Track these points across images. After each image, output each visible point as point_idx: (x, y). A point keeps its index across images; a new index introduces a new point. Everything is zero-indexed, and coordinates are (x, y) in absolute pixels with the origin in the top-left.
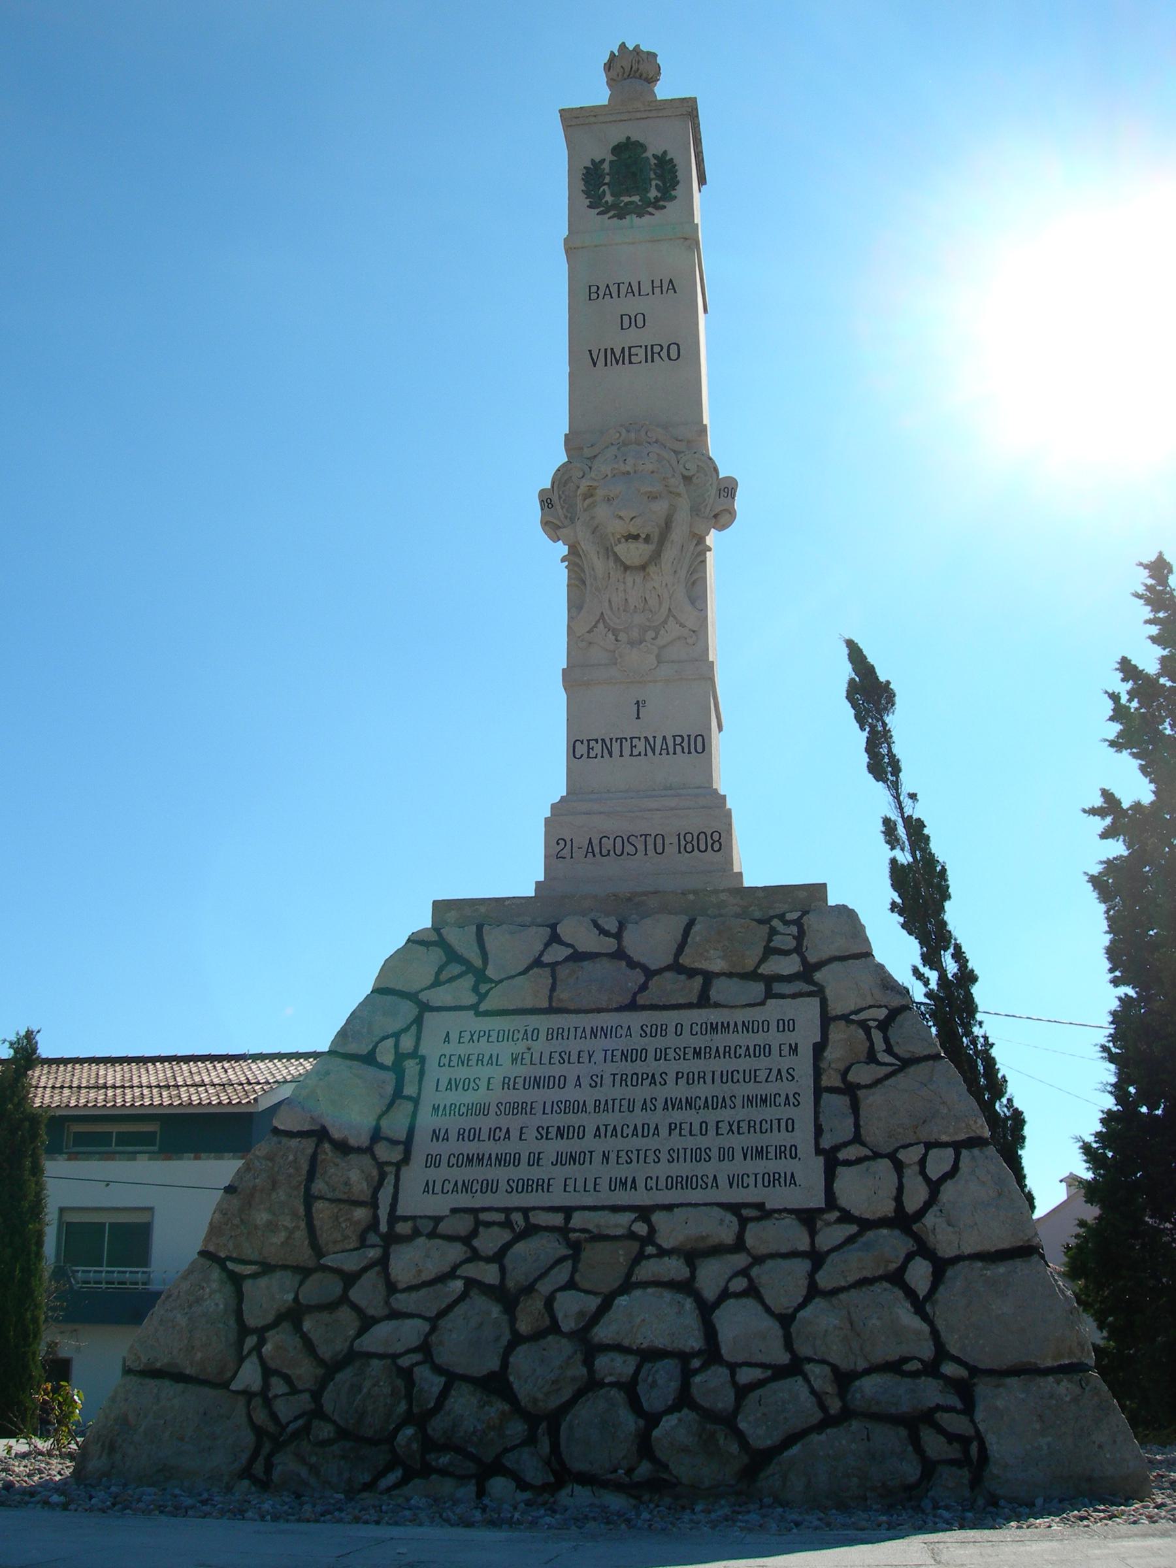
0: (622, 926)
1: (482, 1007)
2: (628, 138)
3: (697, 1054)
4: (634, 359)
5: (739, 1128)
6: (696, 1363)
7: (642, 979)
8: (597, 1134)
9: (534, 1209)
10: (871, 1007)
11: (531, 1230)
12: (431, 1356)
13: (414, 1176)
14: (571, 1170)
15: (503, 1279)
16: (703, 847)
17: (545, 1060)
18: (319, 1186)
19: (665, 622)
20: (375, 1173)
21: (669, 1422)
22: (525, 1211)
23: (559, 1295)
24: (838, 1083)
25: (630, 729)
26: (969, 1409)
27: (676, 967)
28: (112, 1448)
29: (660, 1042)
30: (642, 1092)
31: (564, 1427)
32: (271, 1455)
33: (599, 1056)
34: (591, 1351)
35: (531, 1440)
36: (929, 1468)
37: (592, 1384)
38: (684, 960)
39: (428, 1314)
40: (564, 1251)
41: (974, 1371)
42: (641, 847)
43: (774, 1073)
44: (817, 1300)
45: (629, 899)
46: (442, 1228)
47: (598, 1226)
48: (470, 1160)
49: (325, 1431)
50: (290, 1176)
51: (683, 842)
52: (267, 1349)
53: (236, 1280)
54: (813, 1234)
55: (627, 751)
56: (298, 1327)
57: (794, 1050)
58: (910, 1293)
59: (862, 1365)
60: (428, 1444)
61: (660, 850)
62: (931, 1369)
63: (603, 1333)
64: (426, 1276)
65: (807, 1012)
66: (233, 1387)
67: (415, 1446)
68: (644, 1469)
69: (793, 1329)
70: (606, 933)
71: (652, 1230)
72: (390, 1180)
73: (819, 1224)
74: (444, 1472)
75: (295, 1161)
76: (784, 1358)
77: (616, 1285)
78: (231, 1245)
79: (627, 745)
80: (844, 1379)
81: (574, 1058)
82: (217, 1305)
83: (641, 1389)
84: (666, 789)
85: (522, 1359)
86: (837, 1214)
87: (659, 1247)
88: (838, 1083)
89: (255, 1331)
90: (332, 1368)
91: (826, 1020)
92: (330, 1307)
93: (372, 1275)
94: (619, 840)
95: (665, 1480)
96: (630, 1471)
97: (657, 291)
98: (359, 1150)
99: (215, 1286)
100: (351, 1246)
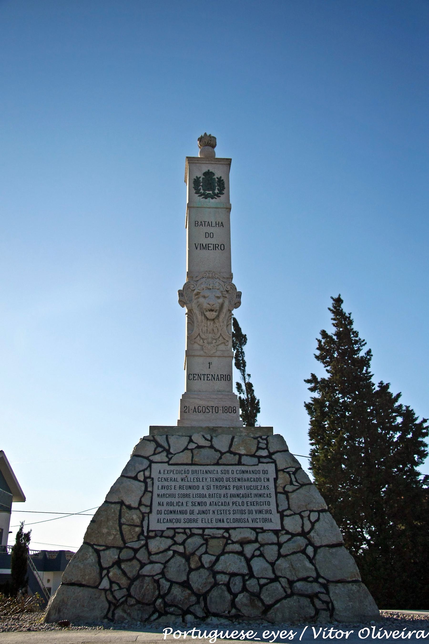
0: (212, 438)
1: (170, 462)
2: (209, 170)
3: (239, 480)
4: (210, 248)
5: (253, 504)
6: (247, 578)
7: (220, 455)
8: (211, 505)
9: (193, 528)
10: (290, 467)
11: (192, 535)
12: (165, 576)
13: (154, 517)
14: (203, 516)
15: (185, 550)
16: (230, 411)
17: (192, 480)
18: (123, 520)
19: (219, 338)
20: (141, 516)
21: (240, 596)
22: (190, 529)
23: (203, 556)
24: (282, 491)
25: (207, 371)
26: (328, 593)
27: (230, 452)
28: (59, 611)
29: (227, 476)
30: (223, 492)
31: (208, 598)
32: (114, 610)
33: (209, 480)
34: (215, 574)
35: (198, 602)
36: (317, 611)
37: (216, 584)
38: (232, 449)
39: (162, 562)
40: (203, 542)
41: (328, 581)
42: (211, 410)
43: (263, 487)
44: (281, 558)
45: (213, 429)
46: (165, 534)
47: (213, 534)
48: (171, 512)
49: (133, 601)
50: (113, 517)
51: (224, 410)
52: (111, 574)
53: (97, 552)
54: (278, 537)
55: (206, 378)
56: (120, 567)
57: (268, 480)
58: (308, 557)
59: (296, 579)
60: (166, 605)
61: (217, 411)
62: (316, 580)
63: (219, 567)
64: (161, 550)
65: (271, 468)
66: (100, 587)
67: (162, 605)
68: (233, 611)
69: (275, 567)
70: (207, 440)
71: (230, 535)
72: (146, 518)
73: (280, 534)
74: (172, 614)
75: (114, 511)
76: (273, 576)
77: (220, 552)
78: (95, 540)
80: (291, 583)
81: (201, 480)
82: (92, 560)
83: (231, 585)
84: (218, 391)
85: (194, 576)
86: (285, 532)
87: (232, 541)
88: (282, 491)
89: (106, 568)
90: (132, 580)
91: (277, 471)
92: (130, 560)
93: (143, 550)
94: (204, 408)
95: (239, 615)
96: (229, 612)
97: (217, 225)
98: (135, 508)
99: (91, 554)
100: (135, 540)
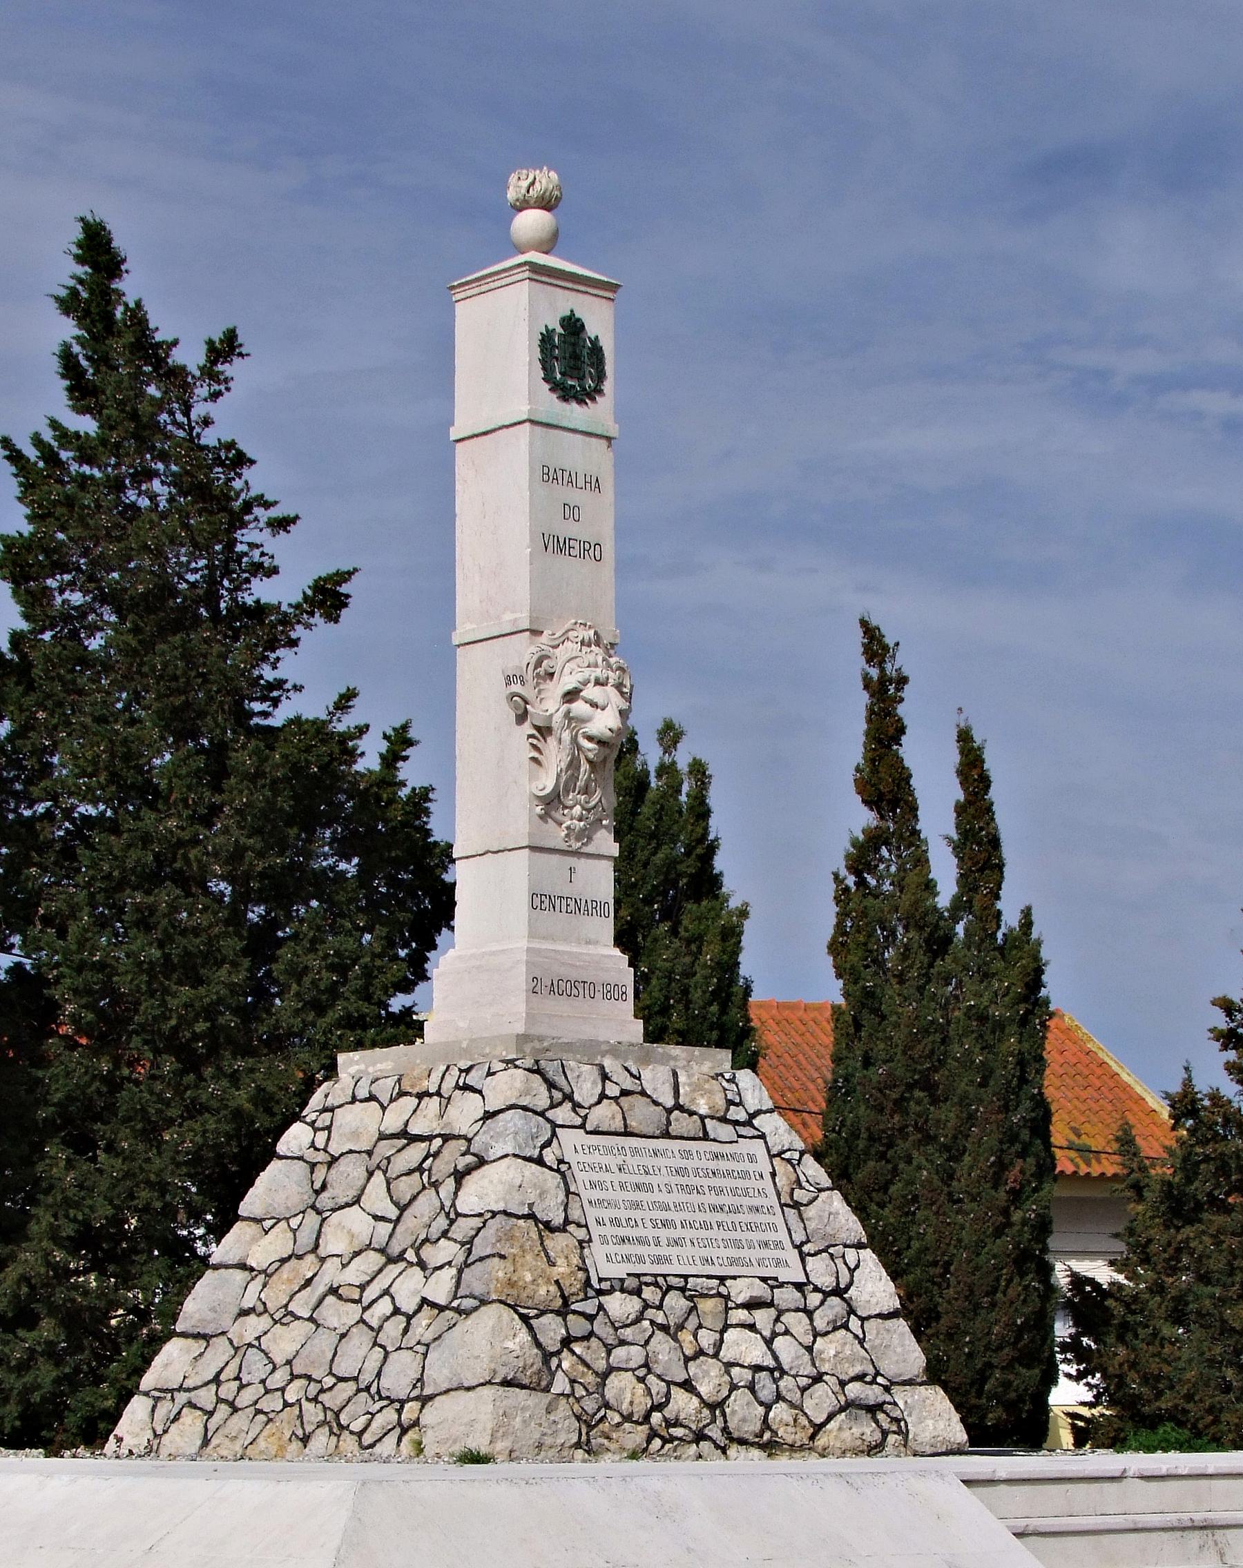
22: (665, 1276)
36: (885, 1434)
37: (733, 1387)
65: (758, 1147)
79: (564, 902)
